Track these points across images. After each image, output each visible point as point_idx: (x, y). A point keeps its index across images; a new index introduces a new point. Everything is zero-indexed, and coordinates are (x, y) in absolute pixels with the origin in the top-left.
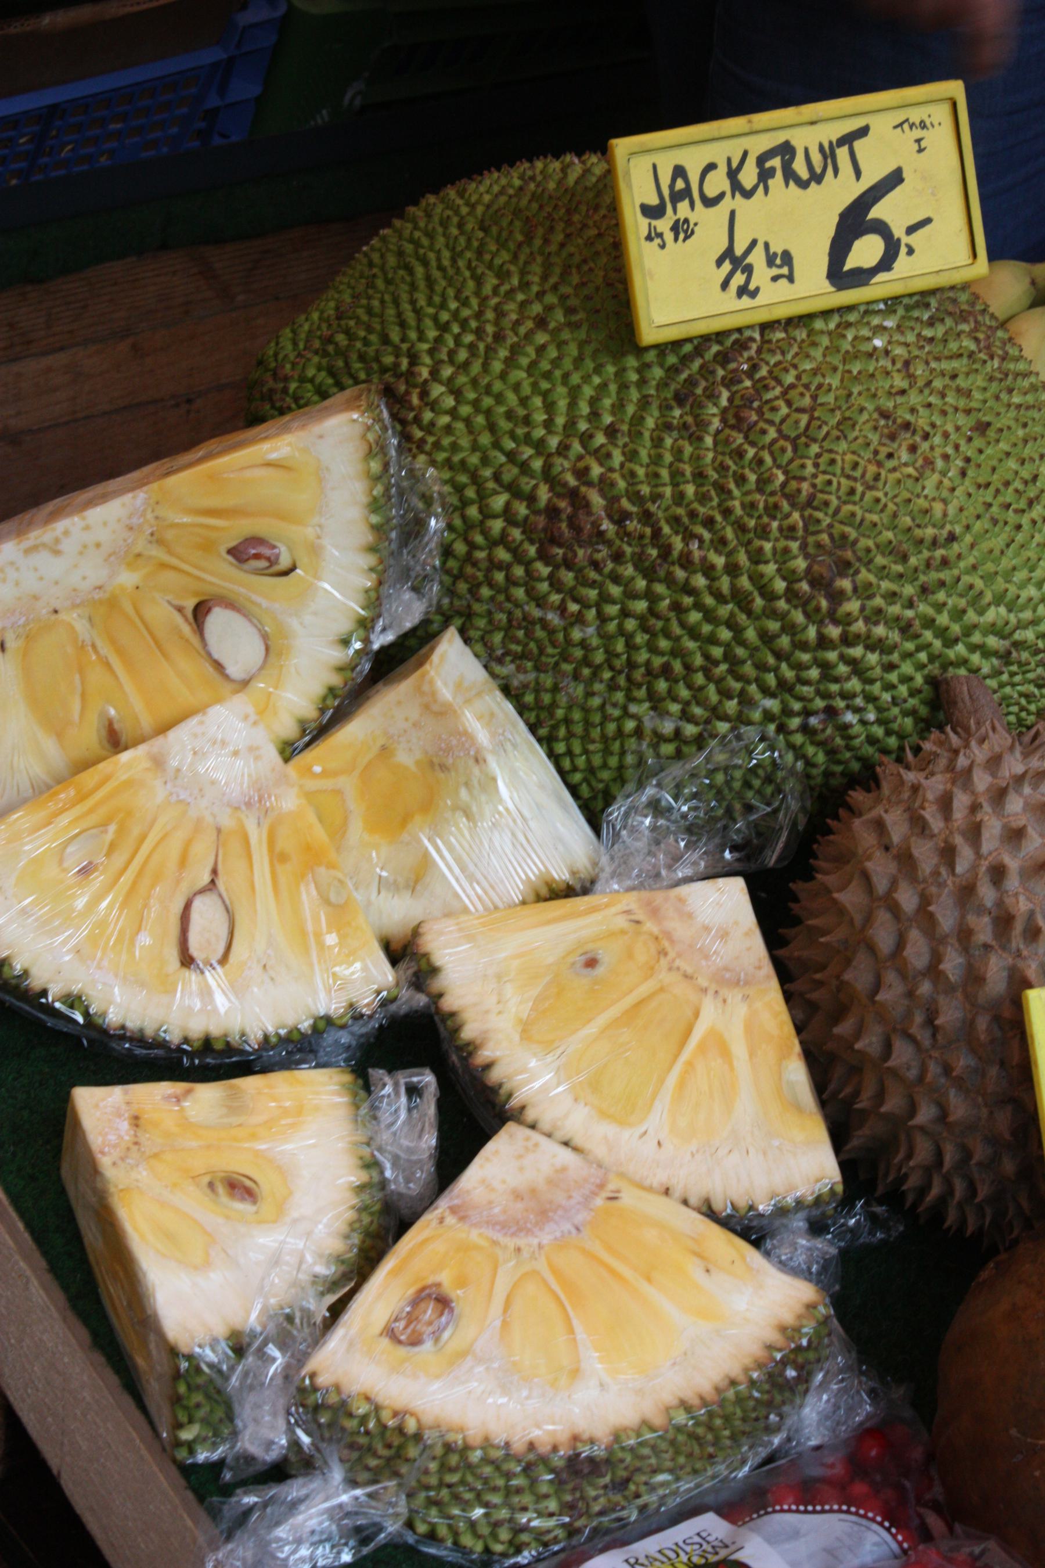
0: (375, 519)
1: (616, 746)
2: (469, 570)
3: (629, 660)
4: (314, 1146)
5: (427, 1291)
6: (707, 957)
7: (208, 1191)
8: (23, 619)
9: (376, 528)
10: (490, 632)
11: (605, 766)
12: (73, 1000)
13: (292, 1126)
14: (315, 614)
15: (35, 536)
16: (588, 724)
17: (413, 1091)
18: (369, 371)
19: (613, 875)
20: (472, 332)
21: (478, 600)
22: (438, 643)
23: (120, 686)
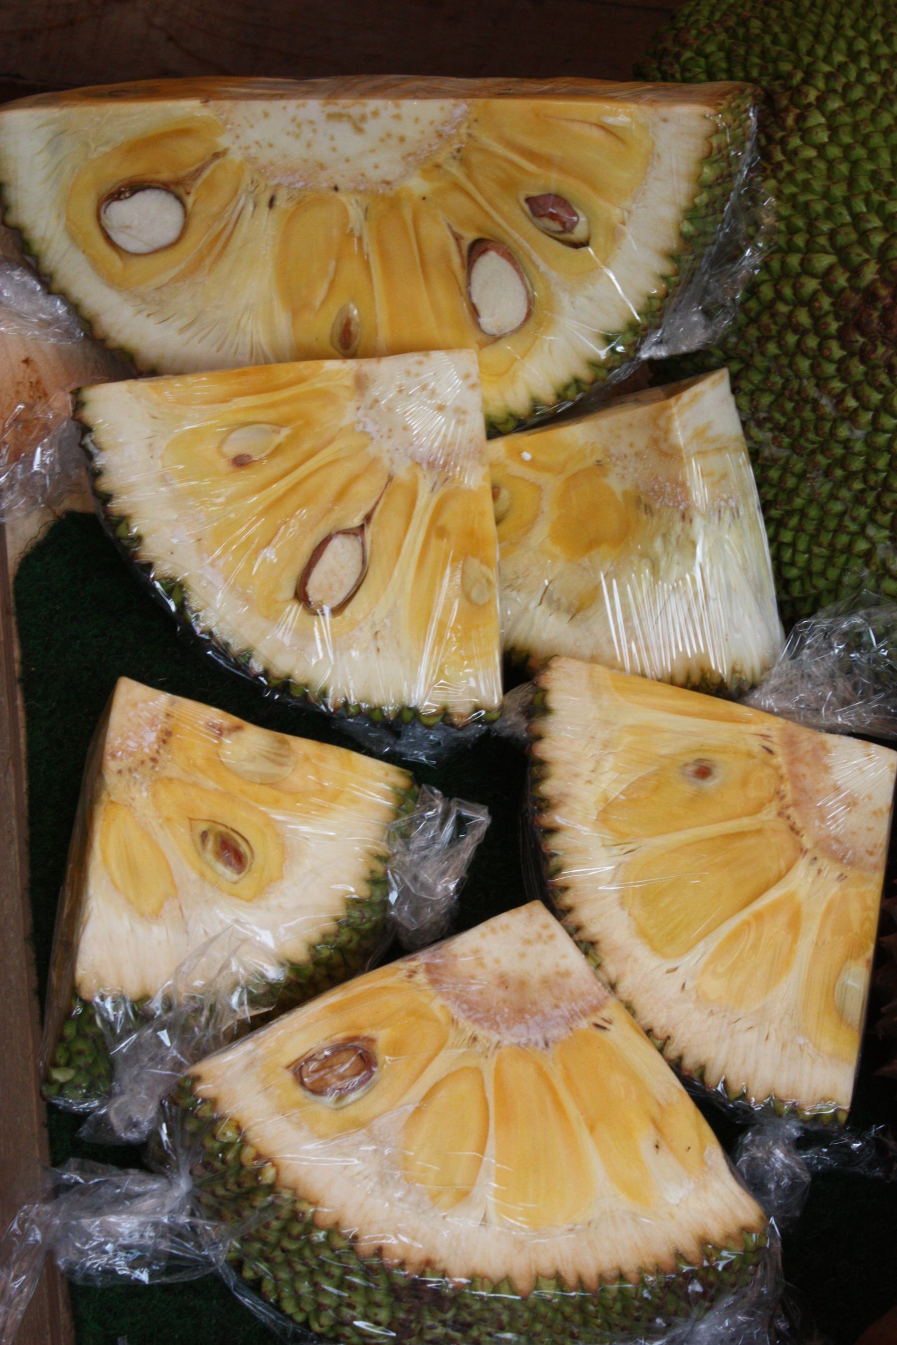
0: (687, 228)
1: (841, 560)
2: (765, 319)
3: (886, 479)
4: (331, 838)
5: (356, 1043)
6: (823, 819)
7: (198, 840)
8: (302, 184)
9: (685, 238)
10: (763, 391)
11: (823, 574)
12: (175, 587)
13: (320, 808)
14: (590, 299)
15: (344, 104)
16: (821, 525)
17: (462, 824)
18: (763, 69)
19: (776, 690)
20: (879, 72)
21: (763, 354)
22: (702, 380)
23: (372, 290)
